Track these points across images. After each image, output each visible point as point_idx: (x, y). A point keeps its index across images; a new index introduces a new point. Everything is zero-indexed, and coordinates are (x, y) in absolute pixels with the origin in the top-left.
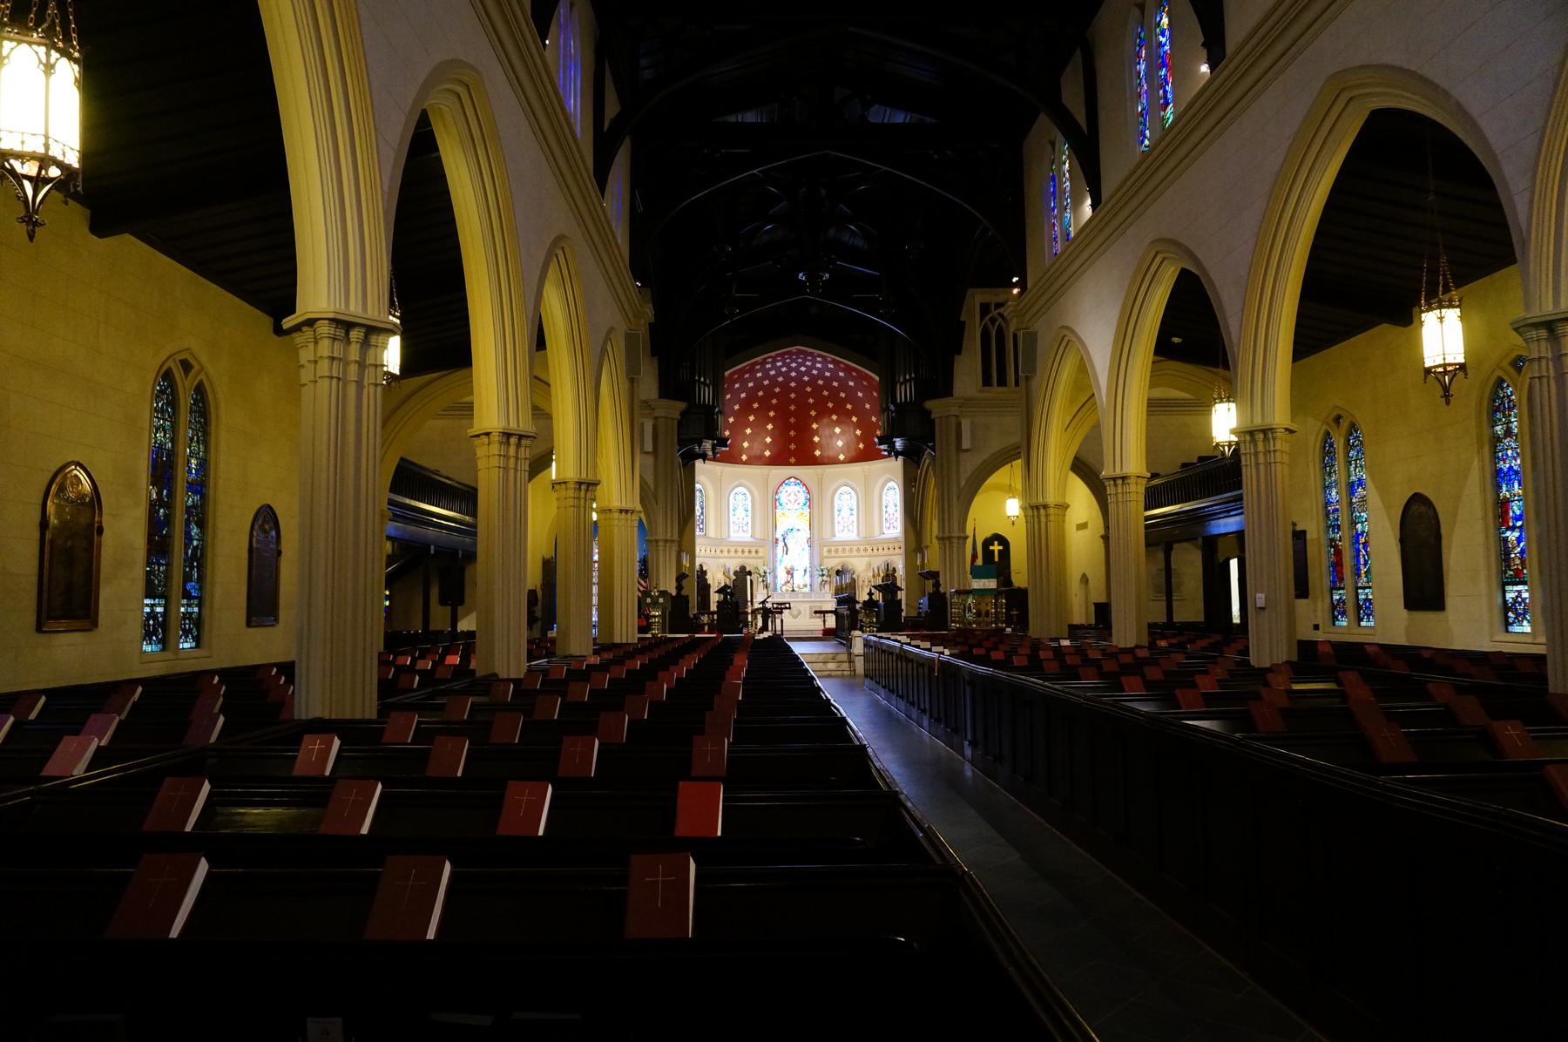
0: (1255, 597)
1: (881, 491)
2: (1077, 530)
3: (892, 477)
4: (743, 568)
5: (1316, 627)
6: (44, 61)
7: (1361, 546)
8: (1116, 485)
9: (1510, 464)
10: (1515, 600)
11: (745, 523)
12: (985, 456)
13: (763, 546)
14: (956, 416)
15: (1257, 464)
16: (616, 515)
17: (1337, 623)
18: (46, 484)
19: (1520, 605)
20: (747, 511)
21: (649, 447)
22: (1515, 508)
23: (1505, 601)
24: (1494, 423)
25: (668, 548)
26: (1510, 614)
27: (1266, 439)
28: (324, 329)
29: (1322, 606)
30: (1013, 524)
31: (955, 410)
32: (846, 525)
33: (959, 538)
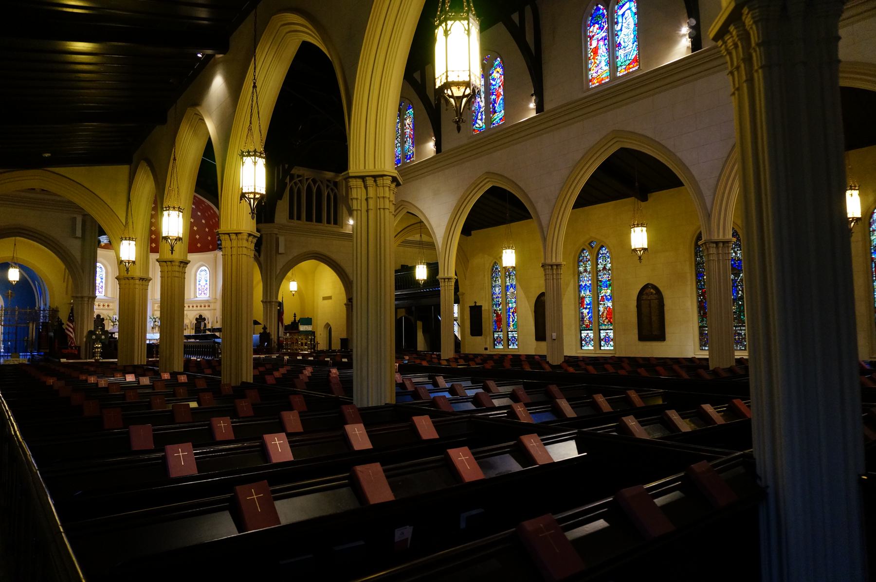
0: (552, 335)
1: (196, 272)
2: (323, 300)
3: (204, 264)
4: (200, 316)
5: (486, 349)
6: (467, 29)
7: (511, 314)
8: (444, 282)
9: (586, 283)
10: (586, 337)
11: (205, 288)
12: (290, 257)
13: (112, 302)
14: (276, 234)
15: (553, 279)
16: (137, 282)
17: (496, 347)
18: (334, 256)
19: (588, 338)
20: (102, 279)
21: (79, 233)
22: (587, 301)
23: (581, 337)
24: (579, 266)
25: (90, 302)
26: (583, 342)
27: (557, 268)
28: (388, 181)
29: (489, 340)
30: (293, 295)
31: (276, 231)
32: (203, 290)
33: (89, 298)
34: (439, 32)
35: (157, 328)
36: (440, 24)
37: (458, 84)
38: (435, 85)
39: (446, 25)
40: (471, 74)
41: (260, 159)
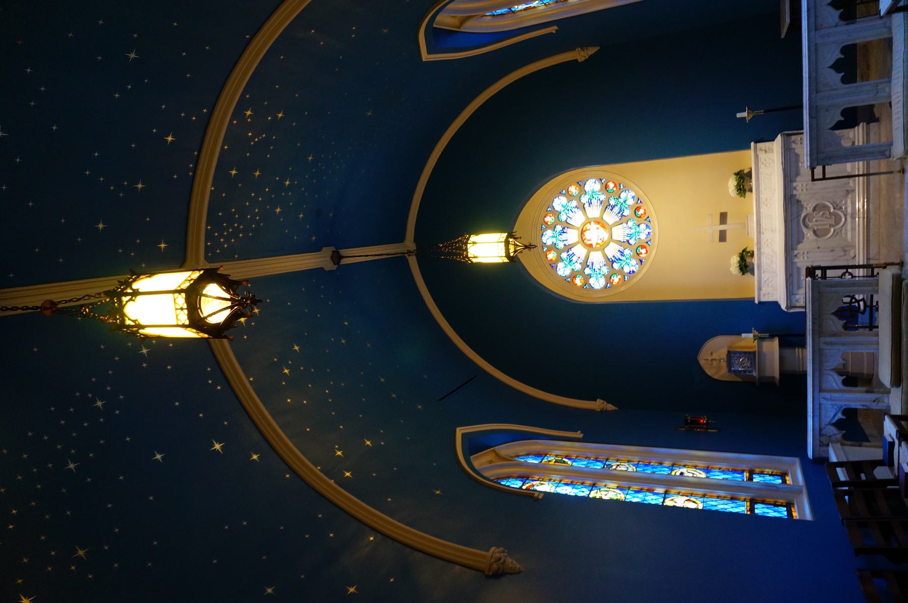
34: (474, 260)
35: (601, 496)
36: (470, 261)
37: (507, 250)
38: (507, 262)
39: (471, 257)
40: (499, 241)
41: (470, 239)
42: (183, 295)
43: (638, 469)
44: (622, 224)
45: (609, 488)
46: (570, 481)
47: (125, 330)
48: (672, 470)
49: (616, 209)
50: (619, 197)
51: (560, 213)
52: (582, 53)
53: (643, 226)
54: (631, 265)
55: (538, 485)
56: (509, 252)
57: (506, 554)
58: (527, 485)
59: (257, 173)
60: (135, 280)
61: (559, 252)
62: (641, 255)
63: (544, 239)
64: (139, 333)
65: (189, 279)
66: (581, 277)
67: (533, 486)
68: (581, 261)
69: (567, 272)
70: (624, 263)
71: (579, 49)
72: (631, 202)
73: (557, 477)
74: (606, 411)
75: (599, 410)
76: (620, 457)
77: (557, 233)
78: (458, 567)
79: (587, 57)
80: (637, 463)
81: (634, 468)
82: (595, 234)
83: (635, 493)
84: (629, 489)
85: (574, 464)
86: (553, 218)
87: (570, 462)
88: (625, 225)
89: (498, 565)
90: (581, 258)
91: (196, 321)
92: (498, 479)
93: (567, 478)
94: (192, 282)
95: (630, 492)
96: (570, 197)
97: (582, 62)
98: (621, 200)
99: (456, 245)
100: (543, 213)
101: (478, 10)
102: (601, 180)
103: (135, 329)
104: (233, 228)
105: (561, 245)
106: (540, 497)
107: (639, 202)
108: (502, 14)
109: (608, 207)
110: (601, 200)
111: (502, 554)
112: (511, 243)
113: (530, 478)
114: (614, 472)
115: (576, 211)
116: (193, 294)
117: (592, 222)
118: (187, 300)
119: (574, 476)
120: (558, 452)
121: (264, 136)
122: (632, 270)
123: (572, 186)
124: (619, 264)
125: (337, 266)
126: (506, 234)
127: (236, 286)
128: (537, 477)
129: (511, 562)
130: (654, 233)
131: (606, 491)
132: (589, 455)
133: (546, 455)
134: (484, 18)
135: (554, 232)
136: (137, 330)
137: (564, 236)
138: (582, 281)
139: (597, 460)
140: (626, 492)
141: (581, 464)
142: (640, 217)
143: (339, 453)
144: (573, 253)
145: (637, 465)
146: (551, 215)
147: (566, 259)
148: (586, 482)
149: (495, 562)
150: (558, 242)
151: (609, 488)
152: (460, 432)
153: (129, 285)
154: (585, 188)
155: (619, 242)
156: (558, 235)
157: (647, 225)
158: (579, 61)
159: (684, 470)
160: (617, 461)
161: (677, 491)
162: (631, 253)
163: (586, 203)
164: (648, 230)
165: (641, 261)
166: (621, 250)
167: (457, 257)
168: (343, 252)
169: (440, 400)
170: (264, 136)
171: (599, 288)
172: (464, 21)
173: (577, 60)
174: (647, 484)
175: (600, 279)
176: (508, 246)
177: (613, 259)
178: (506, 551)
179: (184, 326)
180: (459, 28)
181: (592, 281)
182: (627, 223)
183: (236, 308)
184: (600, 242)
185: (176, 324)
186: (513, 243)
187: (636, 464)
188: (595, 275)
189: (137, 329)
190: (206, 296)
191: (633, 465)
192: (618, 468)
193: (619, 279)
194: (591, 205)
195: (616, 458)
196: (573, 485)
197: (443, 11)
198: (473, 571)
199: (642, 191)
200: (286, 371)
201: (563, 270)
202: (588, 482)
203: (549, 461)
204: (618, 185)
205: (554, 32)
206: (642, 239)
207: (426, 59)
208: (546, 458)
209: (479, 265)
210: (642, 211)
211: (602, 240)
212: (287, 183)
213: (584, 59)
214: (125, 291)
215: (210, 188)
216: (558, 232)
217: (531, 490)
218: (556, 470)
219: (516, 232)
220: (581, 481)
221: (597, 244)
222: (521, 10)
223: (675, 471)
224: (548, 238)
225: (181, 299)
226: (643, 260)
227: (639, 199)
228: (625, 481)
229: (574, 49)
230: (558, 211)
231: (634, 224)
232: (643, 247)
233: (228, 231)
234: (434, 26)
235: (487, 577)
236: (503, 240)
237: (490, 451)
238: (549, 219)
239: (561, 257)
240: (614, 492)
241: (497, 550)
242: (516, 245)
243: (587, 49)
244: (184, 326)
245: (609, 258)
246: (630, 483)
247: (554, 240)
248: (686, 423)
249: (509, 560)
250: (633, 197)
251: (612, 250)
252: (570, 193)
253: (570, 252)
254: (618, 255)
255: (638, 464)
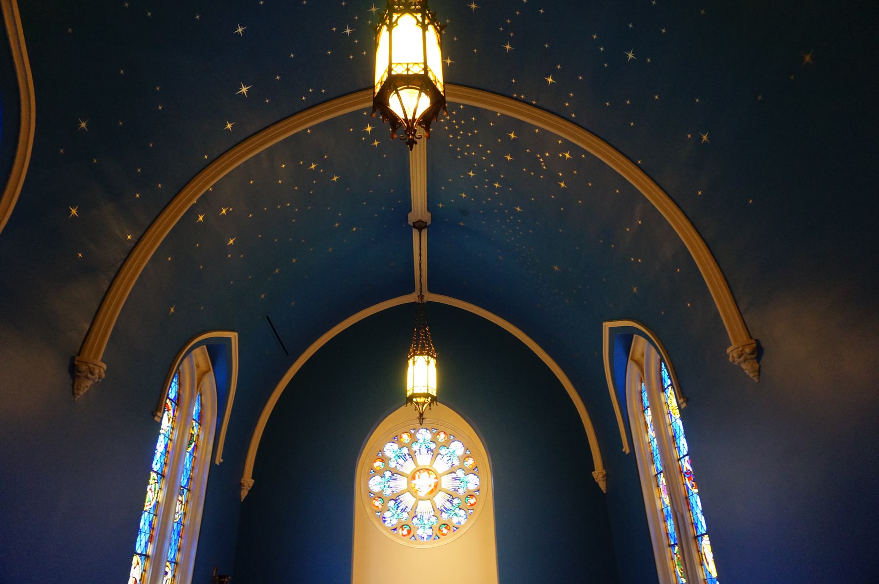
34: (410, 362)
35: (150, 484)
36: (411, 357)
39: (414, 358)
41: (432, 359)
42: (423, 73)
43: (175, 525)
44: (434, 511)
45: (158, 493)
46: (170, 450)
47: (387, 12)
48: (171, 562)
49: (448, 505)
50: (460, 509)
51: (447, 448)
52: (601, 476)
53: (430, 532)
54: (391, 519)
55: (168, 415)
56: (417, 397)
57: (97, 380)
58: (169, 404)
59: (509, 158)
60: (436, 28)
61: (409, 446)
62: (401, 529)
63: (423, 431)
64: (382, 25)
65: (436, 81)
66: (382, 467)
67: (168, 410)
68: (398, 468)
69: (388, 453)
70: (394, 512)
71: (605, 473)
72: (455, 520)
73: (175, 437)
74: (241, 489)
75: (242, 482)
76: (191, 504)
77: (428, 444)
78: (88, 327)
79: (597, 480)
80: (182, 523)
81: (177, 520)
82: (424, 483)
83: (150, 522)
84: (154, 515)
85: (188, 454)
86: (443, 441)
87: (190, 449)
88: (433, 513)
89: (85, 371)
90: (401, 467)
91: (394, 83)
92: (179, 373)
93: (173, 446)
94: (434, 82)
95: (151, 516)
96: (465, 457)
97: (592, 475)
98: (457, 511)
99: (427, 344)
100: (448, 431)
101: (649, 376)
102: (478, 490)
103: (388, 21)
104: (459, 130)
105: (415, 447)
106: (156, 419)
107: (455, 529)
108: (642, 400)
109: (451, 497)
110: (458, 490)
111: (97, 376)
112: (426, 399)
113: (176, 407)
114: (175, 498)
115: (448, 465)
116: (422, 82)
117: (436, 480)
118: (416, 76)
119: (174, 455)
120: (202, 437)
121: (544, 168)
122: (386, 520)
123: (473, 462)
124: (393, 507)
125: (412, 225)
126: (435, 395)
127: (424, 126)
128: (177, 414)
129: (86, 385)
130: (422, 544)
131: (155, 490)
132: (196, 471)
133: (200, 424)
134: (640, 383)
135: (429, 441)
136: (386, 24)
137: (424, 451)
138: (378, 468)
139: (190, 479)
140: (152, 511)
141: (187, 460)
142: (439, 529)
143: (224, 211)
144: (407, 460)
145: (180, 523)
146: (446, 439)
147: (401, 452)
148: (166, 468)
149: (89, 368)
150: (419, 445)
151: (158, 493)
152: (233, 336)
153: (432, 23)
154: (471, 474)
155: (415, 506)
156: (426, 445)
157: (431, 536)
158: (593, 473)
159: (169, 576)
160: (187, 502)
161: (148, 569)
162: (403, 520)
163: (457, 474)
164: (426, 537)
165: (395, 529)
166: (407, 509)
167: (415, 344)
168: (425, 232)
169: (267, 317)
170: (544, 168)
171: (370, 486)
172: (637, 363)
173: (594, 470)
174: (159, 536)
175: (379, 486)
176: (424, 397)
177: (399, 501)
178: (100, 380)
179: (390, 69)
180: (632, 359)
181: (377, 478)
182: (434, 516)
183: (406, 125)
184: (417, 488)
185: (393, 61)
186: (426, 401)
187: (181, 522)
188: (383, 482)
189: (388, 24)
190: (420, 95)
191: (180, 519)
192: (179, 503)
193: (378, 506)
194: (454, 480)
195: (189, 500)
196: (166, 453)
197: (650, 344)
198: (80, 344)
199: (464, 534)
200: (313, 166)
201: (390, 449)
202: (166, 470)
203: (193, 428)
204: (471, 508)
205: (624, 450)
206: (418, 531)
207: (605, 326)
208: (197, 424)
209: (405, 366)
210: (445, 531)
211: (418, 490)
212: (497, 185)
213: (595, 477)
214: (426, 17)
215: (500, 112)
216: (429, 445)
217: (165, 408)
218: (183, 434)
219: (437, 405)
220: (168, 462)
221: (415, 484)
222: (645, 419)
223: (169, 566)
224: (424, 435)
225: (418, 70)
226: (396, 532)
227: (457, 528)
228: (164, 510)
229: (604, 468)
230: (449, 446)
231: (433, 523)
232: (409, 532)
233: (456, 124)
234: (635, 335)
235: (73, 359)
236: (430, 392)
237: (209, 365)
238: (442, 437)
239: (403, 447)
240: (153, 498)
241: (102, 371)
242: (424, 404)
243: (604, 480)
244: (390, 69)
245: (400, 497)
246: (161, 517)
247: (421, 441)
248: (221, 577)
249: (89, 383)
250: (459, 523)
251: (408, 500)
252: (467, 459)
253: (408, 457)
254: (402, 506)
255: (181, 524)
